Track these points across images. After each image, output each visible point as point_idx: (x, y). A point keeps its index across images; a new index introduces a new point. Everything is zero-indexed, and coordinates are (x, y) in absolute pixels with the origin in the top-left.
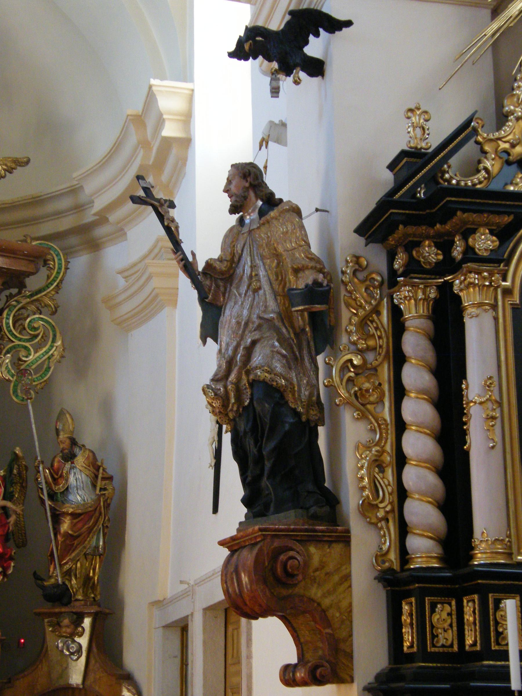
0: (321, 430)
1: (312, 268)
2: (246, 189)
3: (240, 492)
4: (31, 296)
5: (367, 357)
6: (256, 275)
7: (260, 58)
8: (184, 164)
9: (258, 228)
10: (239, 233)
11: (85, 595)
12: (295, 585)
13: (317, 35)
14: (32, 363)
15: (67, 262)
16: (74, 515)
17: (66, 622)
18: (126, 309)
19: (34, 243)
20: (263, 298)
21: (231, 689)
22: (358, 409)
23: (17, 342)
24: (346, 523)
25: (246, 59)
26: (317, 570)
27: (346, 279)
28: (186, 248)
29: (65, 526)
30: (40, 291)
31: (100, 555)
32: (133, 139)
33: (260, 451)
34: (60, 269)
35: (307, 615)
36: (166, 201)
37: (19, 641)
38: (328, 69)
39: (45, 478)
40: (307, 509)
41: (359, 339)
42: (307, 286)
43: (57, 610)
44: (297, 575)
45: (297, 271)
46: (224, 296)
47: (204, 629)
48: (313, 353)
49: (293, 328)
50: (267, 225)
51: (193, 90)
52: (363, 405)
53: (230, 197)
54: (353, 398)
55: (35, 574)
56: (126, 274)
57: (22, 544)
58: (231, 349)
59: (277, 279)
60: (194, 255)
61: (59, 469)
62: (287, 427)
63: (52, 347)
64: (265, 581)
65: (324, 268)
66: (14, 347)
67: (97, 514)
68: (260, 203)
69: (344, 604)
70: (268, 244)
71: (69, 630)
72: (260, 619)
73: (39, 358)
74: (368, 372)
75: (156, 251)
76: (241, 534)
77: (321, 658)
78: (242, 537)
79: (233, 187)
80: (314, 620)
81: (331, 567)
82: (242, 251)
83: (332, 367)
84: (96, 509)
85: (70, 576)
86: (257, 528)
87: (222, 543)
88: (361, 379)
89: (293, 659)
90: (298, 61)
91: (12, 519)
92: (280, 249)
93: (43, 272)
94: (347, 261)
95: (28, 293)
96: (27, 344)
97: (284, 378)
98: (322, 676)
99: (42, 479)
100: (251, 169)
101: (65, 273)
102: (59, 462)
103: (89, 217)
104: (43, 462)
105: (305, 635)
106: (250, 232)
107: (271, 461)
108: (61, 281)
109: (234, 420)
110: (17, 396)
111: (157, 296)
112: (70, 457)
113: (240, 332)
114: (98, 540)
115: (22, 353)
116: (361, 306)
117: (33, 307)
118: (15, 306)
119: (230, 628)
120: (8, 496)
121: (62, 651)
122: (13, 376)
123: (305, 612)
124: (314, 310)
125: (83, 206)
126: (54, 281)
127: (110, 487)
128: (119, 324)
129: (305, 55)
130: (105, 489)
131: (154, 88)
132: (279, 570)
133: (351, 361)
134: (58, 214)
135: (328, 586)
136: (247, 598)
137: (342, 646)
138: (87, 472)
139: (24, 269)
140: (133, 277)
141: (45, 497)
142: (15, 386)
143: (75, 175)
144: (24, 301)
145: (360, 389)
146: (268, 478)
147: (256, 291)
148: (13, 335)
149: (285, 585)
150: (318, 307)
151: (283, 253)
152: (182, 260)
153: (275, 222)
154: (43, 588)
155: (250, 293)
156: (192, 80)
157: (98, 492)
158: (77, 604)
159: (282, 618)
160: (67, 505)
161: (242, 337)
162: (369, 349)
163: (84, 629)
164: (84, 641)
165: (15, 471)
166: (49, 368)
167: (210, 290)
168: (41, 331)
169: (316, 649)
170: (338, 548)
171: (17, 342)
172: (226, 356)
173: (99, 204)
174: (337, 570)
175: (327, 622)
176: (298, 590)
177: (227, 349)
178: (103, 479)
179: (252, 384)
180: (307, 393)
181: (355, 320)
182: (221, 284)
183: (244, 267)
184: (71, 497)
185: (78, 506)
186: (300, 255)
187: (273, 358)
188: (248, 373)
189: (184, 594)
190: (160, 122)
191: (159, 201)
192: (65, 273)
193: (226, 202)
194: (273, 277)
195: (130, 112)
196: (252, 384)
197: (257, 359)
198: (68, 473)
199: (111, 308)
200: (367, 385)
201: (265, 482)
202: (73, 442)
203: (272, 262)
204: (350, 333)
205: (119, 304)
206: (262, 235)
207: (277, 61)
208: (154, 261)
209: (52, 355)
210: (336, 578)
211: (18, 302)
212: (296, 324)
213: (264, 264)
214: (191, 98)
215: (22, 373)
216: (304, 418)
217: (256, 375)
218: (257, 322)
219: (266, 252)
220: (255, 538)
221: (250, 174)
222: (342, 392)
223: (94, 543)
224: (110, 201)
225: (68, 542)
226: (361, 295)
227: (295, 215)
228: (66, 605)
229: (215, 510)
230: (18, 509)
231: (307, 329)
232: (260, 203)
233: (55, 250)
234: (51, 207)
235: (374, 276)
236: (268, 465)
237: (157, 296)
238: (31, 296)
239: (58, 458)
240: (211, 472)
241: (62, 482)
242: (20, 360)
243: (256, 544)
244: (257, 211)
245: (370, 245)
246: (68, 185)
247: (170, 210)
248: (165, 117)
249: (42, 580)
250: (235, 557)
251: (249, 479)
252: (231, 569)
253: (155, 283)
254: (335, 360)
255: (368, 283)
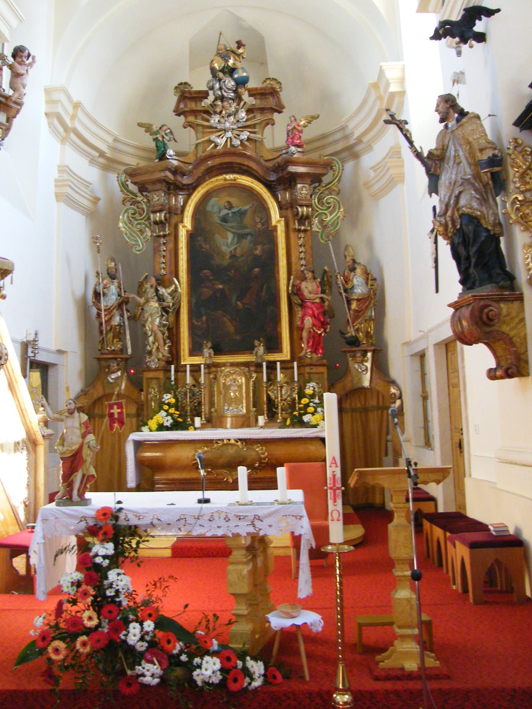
0: (501, 238)
1: (490, 148)
2: (448, 108)
3: (457, 276)
4: (326, 186)
5: (526, 195)
6: (458, 155)
7: (448, 37)
8: (402, 106)
9: (457, 129)
10: (446, 133)
11: (367, 341)
12: (493, 325)
13: (480, 19)
14: (329, 221)
15: (343, 166)
16: (358, 300)
17: (358, 355)
18: (376, 187)
19: (325, 158)
20: (463, 168)
21: (452, 385)
22: (523, 225)
23: (320, 211)
24: (520, 289)
25: (440, 39)
26: (505, 316)
27: (510, 152)
28: (417, 145)
29: (354, 306)
30: (330, 183)
31: (373, 320)
32: (373, 96)
33: (468, 252)
34: (339, 170)
35: (502, 341)
36: (403, 121)
37: (336, 366)
38: (488, 37)
39: (341, 281)
40: (497, 283)
41: (521, 185)
42: (489, 158)
43: (353, 349)
44: (495, 320)
45: (481, 150)
46: (440, 168)
47: (435, 355)
48: (494, 196)
49: (482, 182)
50: (461, 127)
51: (404, 65)
52: (526, 222)
53: (439, 114)
54: (520, 219)
55: (340, 331)
56: (375, 169)
57: (332, 317)
58: (447, 198)
59: (470, 156)
60: (421, 148)
61: (348, 276)
62: (483, 238)
63: (338, 212)
64: (477, 324)
65: (497, 147)
66: (319, 214)
67: (370, 299)
68: (456, 115)
69: (522, 334)
70: (463, 138)
71: (360, 359)
72: (474, 345)
73: (333, 218)
74: (527, 204)
75: (390, 154)
76: (461, 299)
77: (510, 364)
78: (462, 301)
79: (440, 108)
80: (506, 344)
81: (514, 314)
82: (449, 142)
83: (506, 202)
84: (368, 297)
85: (358, 331)
86: (470, 295)
87: (450, 306)
88: (524, 208)
89: (494, 366)
90: (471, 35)
91: (326, 303)
92: (471, 139)
93: (331, 173)
94: (510, 142)
95: (324, 185)
96: (326, 212)
97: (480, 211)
98: (513, 373)
99: (339, 282)
100: (450, 97)
101: (342, 172)
102: (348, 272)
103: (352, 141)
104: (339, 273)
105: (500, 352)
106: (452, 132)
107: (475, 258)
108: (341, 176)
109: (451, 237)
110: (323, 240)
111: (393, 178)
112: (353, 269)
113: (452, 188)
114: (371, 312)
115: (323, 217)
116: (520, 167)
117: (327, 192)
118: (318, 193)
119: (449, 354)
120: (323, 292)
121: (357, 370)
122: (320, 229)
123: (500, 340)
124: (494, 171)
125: (349, 135)
126: (337, 177)
127: (375, 284)
128: (373, 196)
129: (474, 31)
130: (372, 285)
131: (383, 67)
132: (485, 317)
133: (517, 198)
134: (336, 142)
135: (513, 324)
136: (467, 335)
137: (523, 357)
138: (363, 277)
139: (321, 172)
140: (379, 170)
141: (342, 291)
142: (322, 235)
143: (343, 120)
144: (322, 189)
145: (524, 214)
146: (474, 267)
147: (459, 164)
148: (318, 208)
149: (490, 326)
150: (496, 169)
151: (473, 141)
152: (415, 152)
153: (466, 125)
154: (346, 338)
155: (455, 165)
156: (403, 60)
157: (369, 287)
158: (365, 345)
159: (486, 344)
160: (354, 295)
161: (453, 192)
162: (527, 190)
163: (368, 359)
164: (368, 364)
165: (325, 279)
166: (338, 223)
167: (432, 166)
168: (332, 204)
169: (507, 359)
170: (516, 304)
171: (320, 211)
172: (445, 202)
173: (357, 134)
174: (517, 316)
175: (512, 344)
176: (495, 328)
177: (445, 198)
178: (372, 280)
179: (461, 216)
180: (492, 219)
181: (517, 175)
182: (438, 162)
183: (450, 151)
184: (355, 291)
185: (360, 295)
186: (482, 142)
187: (472, 200)
188: (458, 210)
189: (422, 338)
190: (388, 84)
191: (399, 121)
192: (342, 172)
193: (437, 117)
194: (468, 156)
195: (371, 82)
196: (461, 216)
197: (463, 202)
198: (353, 278)
199: (369, 188)
200: (527, 211)
201: (472, 270)
202: (354, 261)
203: (467, 147)
204: (515, 183)
205: (372, 185)
206: (459, 132)
207: (458, 37)
208: (391, 160)
209: (339, 216)
210: (517, 320)
211: (319, 190)
212: (483, 180)
213: (462, 148)
214: (403, 70)
215: (325, 227)
216: (492, 233)
217: (463, 211)
218: (461, 181)
219: (462, 142)
220: (470, 300)
221: (449, 100)
222: (513, 216)
223: (369, 314)
224: (366, 128)
225: (356, 314)
226: (519, 161)
227: (477, 119)
228: (358, 346)
229: (437, 291)
230: (329, 298)
231: (490, 182)
232: (456, 115)
233: (336, 161)
234: (331, 139)
235: (526, 149)
236: (473, 260)
237: (393, 178)
238: (326, 186)
239: (347, 271)
240: (433, 271)
241: (350, 283)
242: (323, 220)
243: (469, 304)
244: (455, 120)
245: (523, 131)
246: (340, 126)
247: (406, 125)
248: (390, 81)
249: (344, 334)
250: (458, 312)
251: (463, 269)
252: (456, 319)
253: (392, 171)
254: (507, 199)
255: (523, 153)
